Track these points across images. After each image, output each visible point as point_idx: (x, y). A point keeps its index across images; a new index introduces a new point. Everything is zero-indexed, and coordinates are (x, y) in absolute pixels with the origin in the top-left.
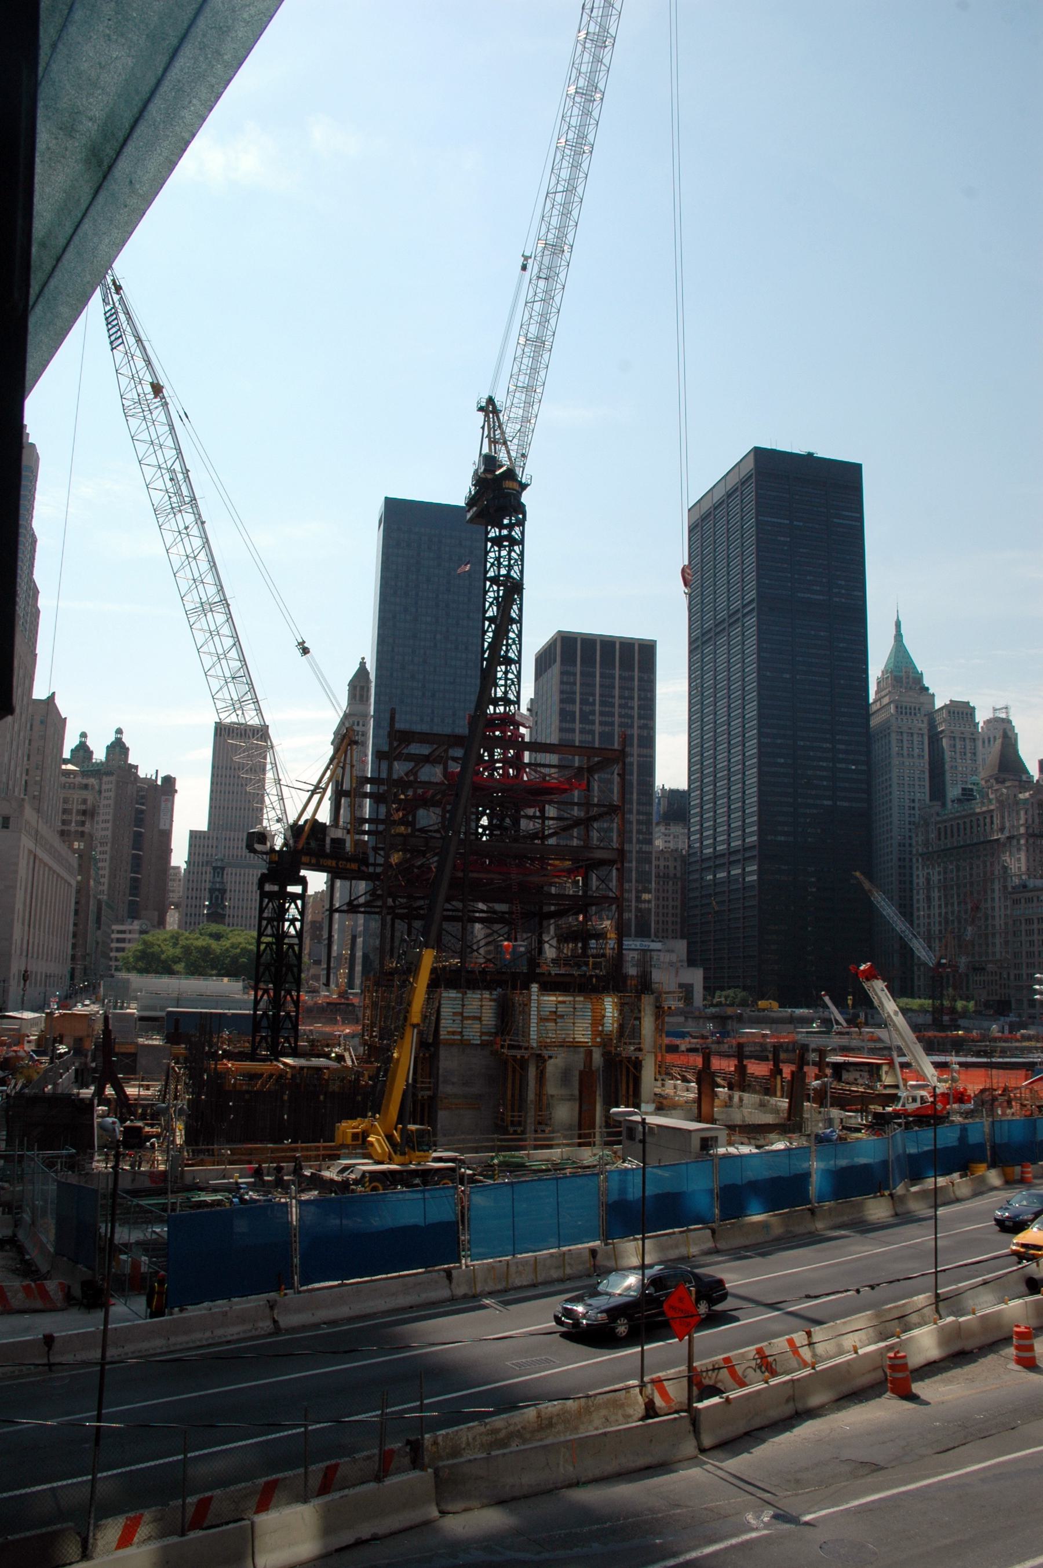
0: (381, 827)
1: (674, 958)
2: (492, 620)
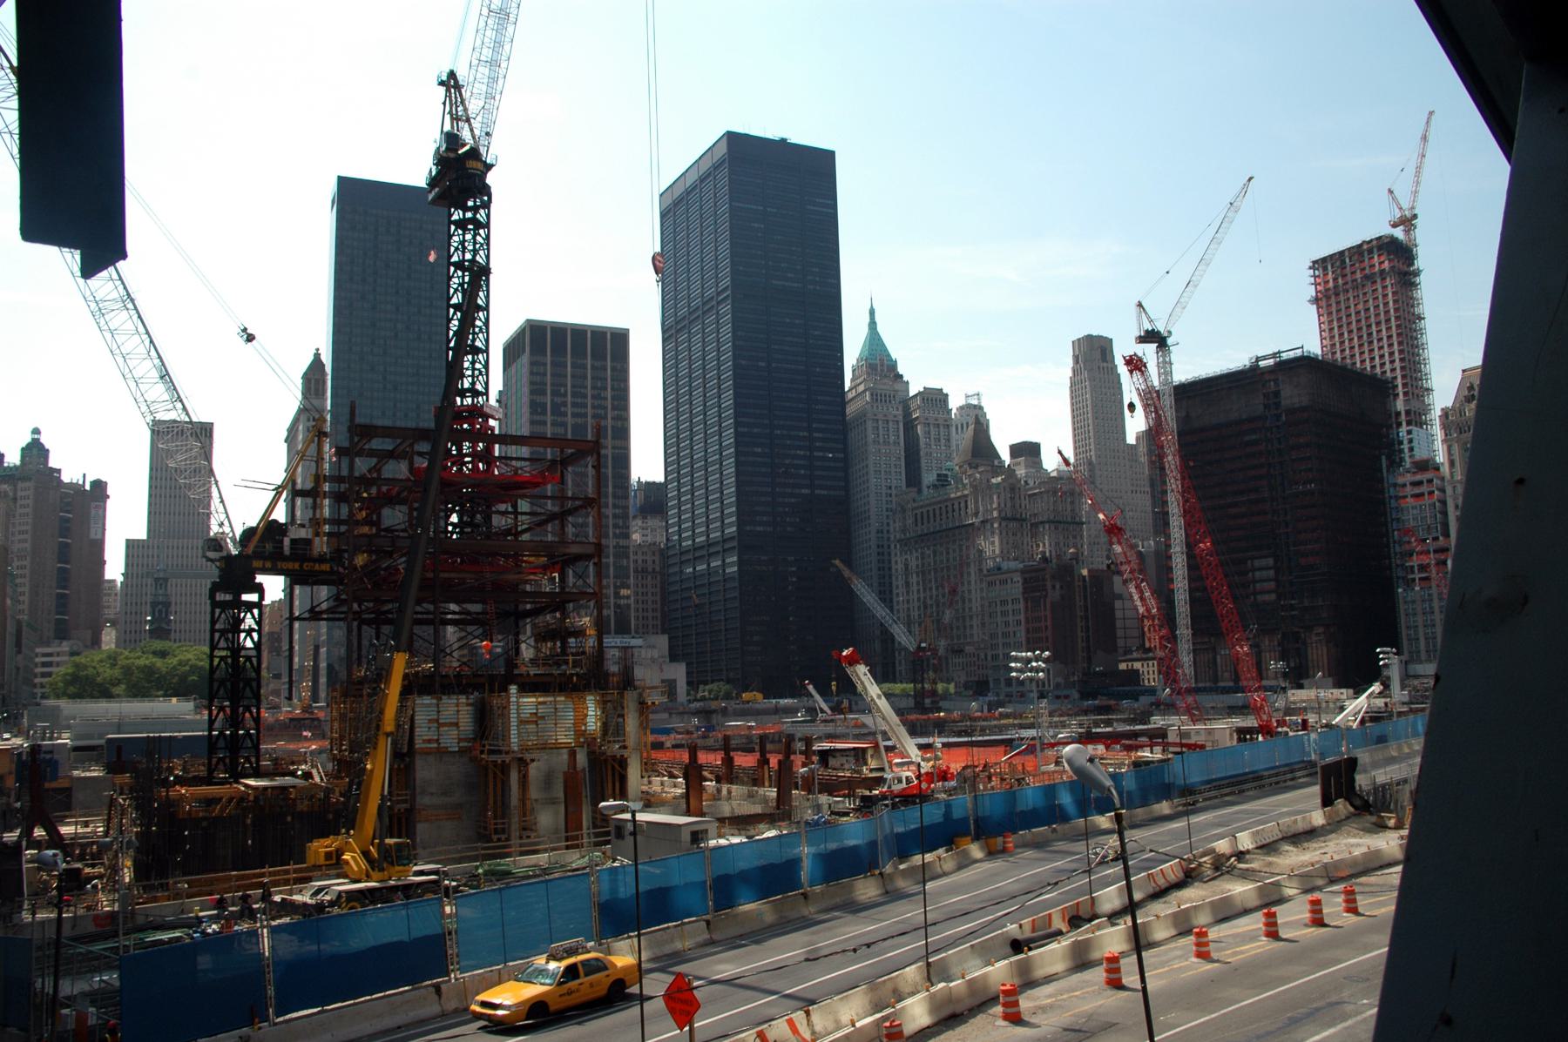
0: (343, 528)
1: (656, 654)
2: (457, 307)
